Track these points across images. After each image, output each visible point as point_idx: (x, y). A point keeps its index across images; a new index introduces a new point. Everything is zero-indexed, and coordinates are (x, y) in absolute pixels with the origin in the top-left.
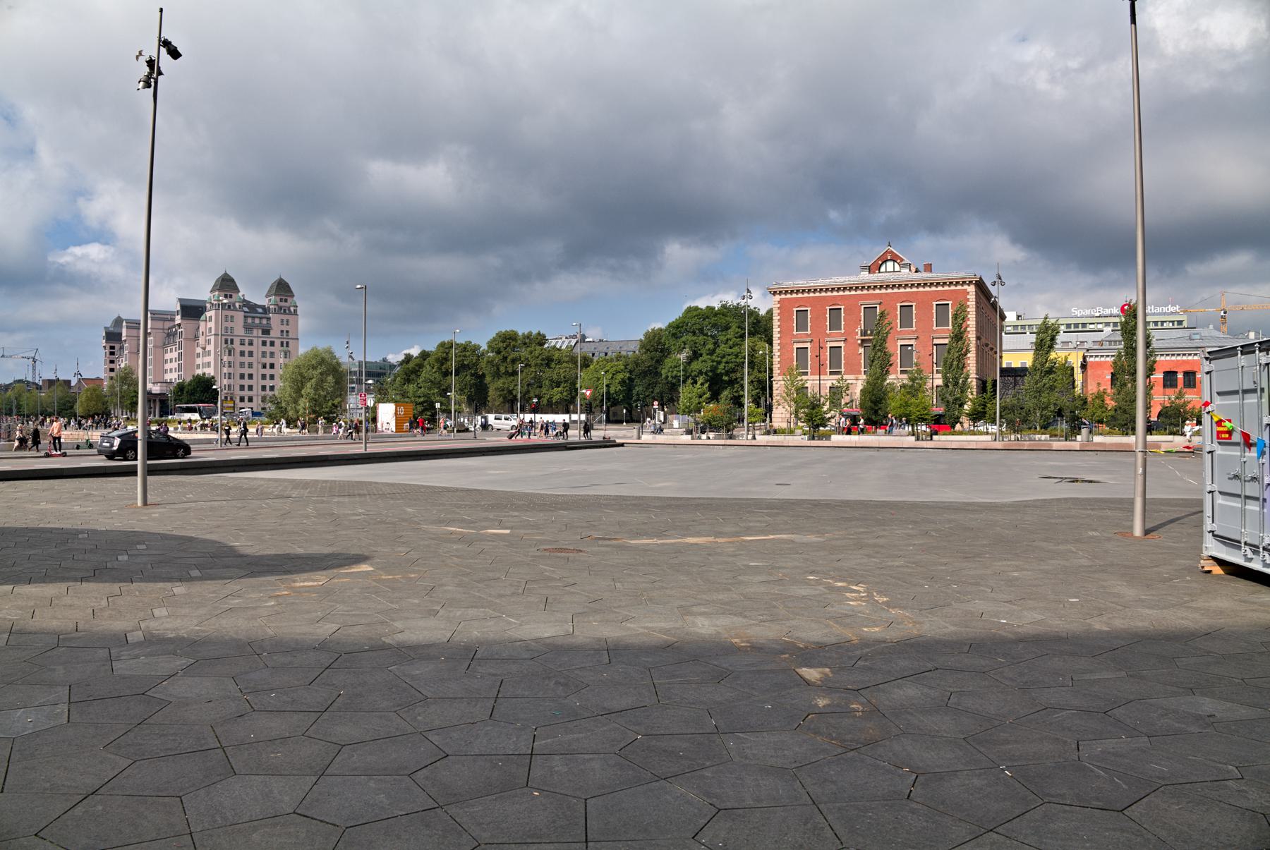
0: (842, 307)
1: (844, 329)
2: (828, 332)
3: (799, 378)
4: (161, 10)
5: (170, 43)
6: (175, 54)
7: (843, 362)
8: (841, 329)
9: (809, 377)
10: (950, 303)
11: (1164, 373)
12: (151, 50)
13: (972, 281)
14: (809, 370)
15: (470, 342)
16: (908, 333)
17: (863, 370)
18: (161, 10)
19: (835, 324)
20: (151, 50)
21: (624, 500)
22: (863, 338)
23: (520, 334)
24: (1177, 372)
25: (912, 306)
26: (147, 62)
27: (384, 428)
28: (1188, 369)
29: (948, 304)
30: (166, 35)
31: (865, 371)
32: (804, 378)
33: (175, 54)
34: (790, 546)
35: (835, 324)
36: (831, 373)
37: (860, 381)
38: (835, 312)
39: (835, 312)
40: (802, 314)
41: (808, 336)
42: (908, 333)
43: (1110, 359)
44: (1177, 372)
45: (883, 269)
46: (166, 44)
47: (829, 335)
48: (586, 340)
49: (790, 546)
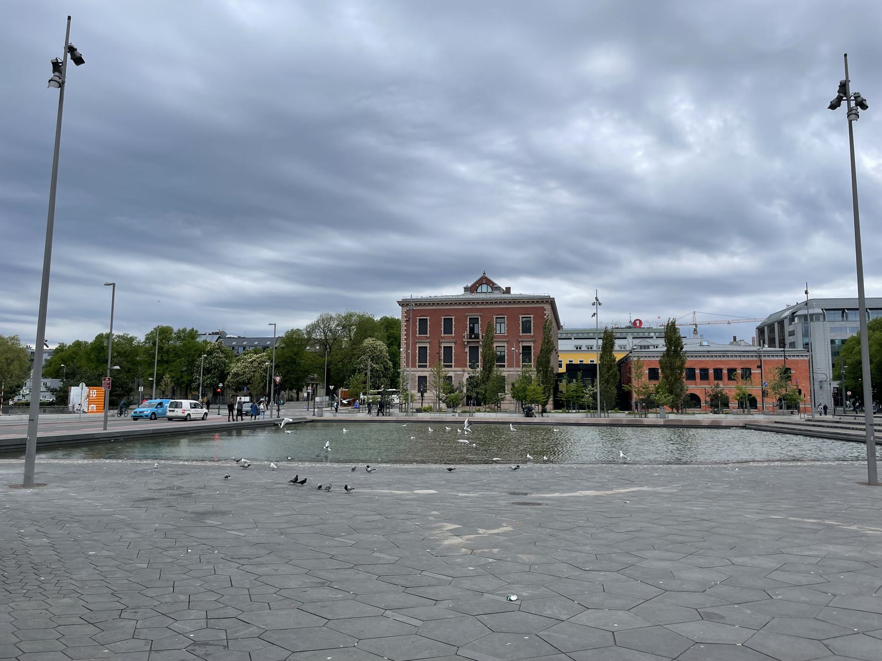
0: (453, 317)
1: (533, 332)
2: (442, 335)
3: (443, 369)
4: (69, 18)
5: (76, 50)
6: (79, 61)
7: (453, 358)
8: (452, 334)
9: (453, 369)
10: (428, 318)
11: (649, 369)
12: (59, 53)
13: (548, 301)
14: (453, 364)
15: (102, 334)
16: (527, 337)
17: (468, 364)
18: (69, 18)
19: (448, 330)
20: (59, 53)
21: (194, 468)
22: (469, 340)
23: (175, 330)
24: (695, 369)
25: (504, 318)
26: (53, 63)
27: (75, 409)
28: (703, 366)
29: (427, 319)
30: (73, 42)
31: (469, 365)
32: (501, 369)
33: (79, 61)
34: (693, 473)
35: (448, 330)
36: (419, 366)
37: (466, 372)
38: (448, 322)
39: (448, 322)
40: (423, 322)
41: (427, 338)
42: (527, 337)
43: (658, 359)
44: (695, 369)
45: (479, 290)
46: (71, 50)
47: (442, 338)
48: (227, 336)
49: (693, 473)
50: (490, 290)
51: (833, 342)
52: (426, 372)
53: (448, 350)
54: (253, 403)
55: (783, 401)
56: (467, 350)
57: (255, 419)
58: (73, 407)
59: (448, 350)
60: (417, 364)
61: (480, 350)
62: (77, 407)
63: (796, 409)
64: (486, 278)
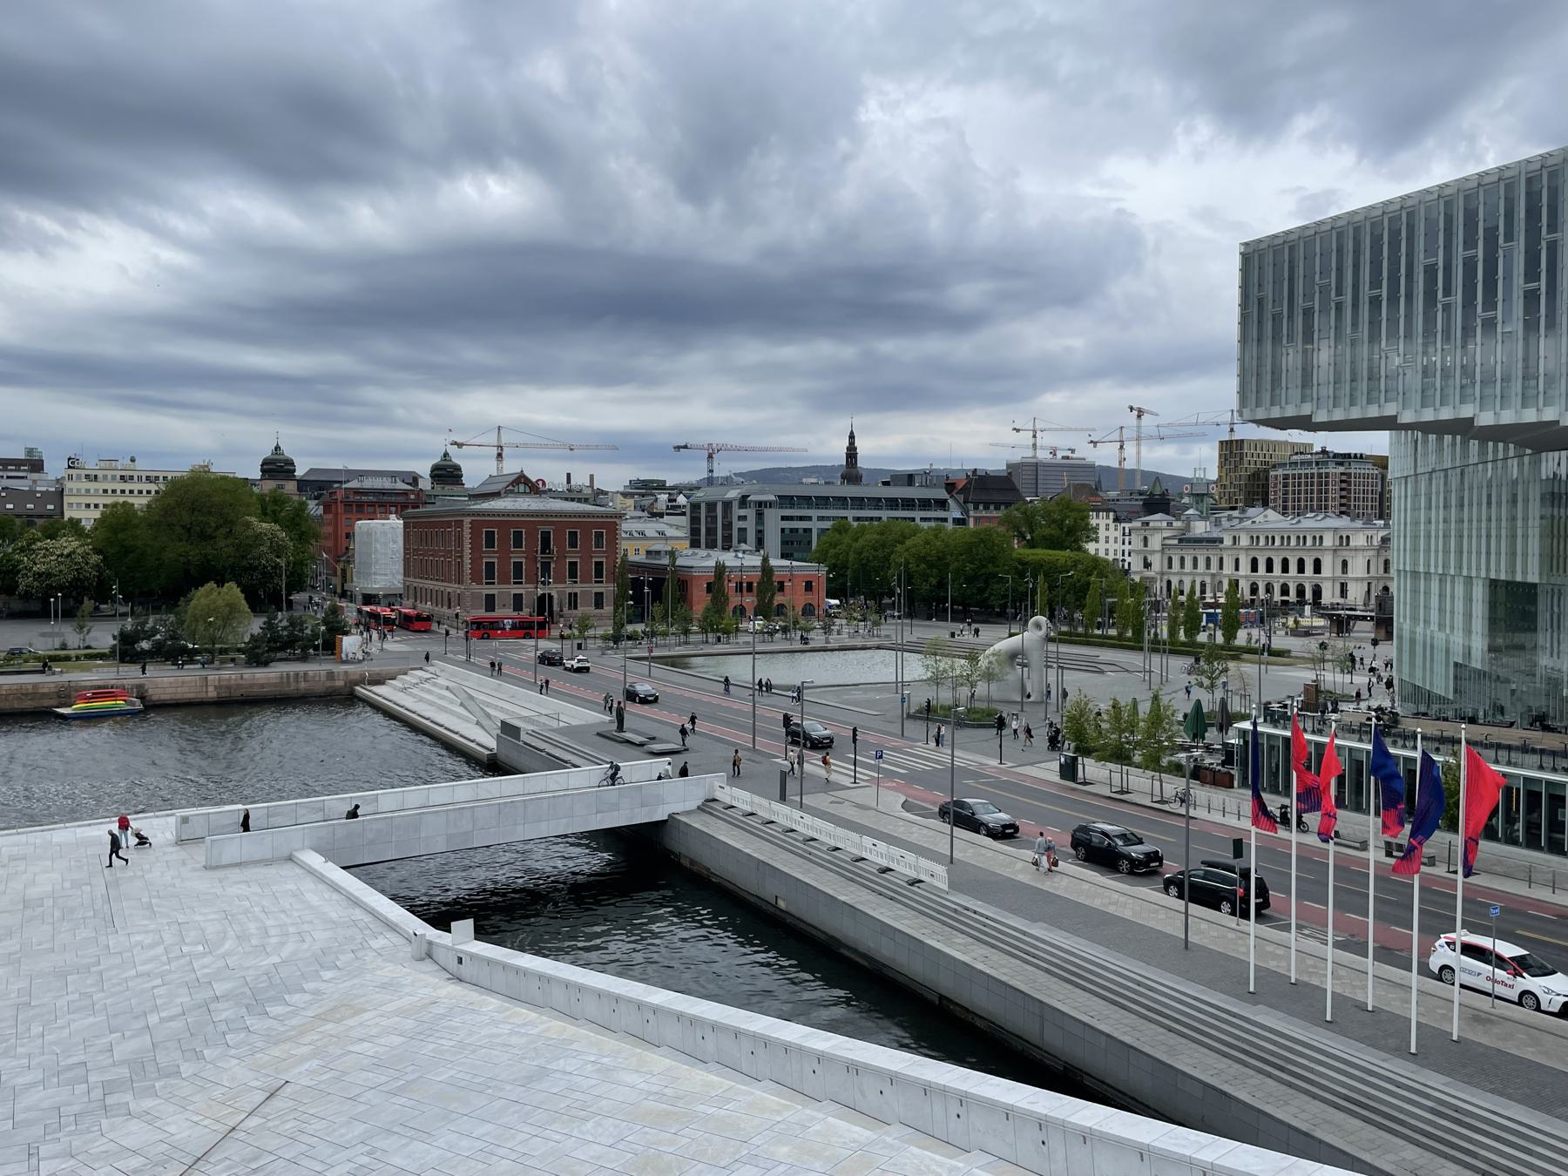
9: (524, 585)
19: (518, 544)
35: (518, 544)
36: (487, 583)
38: (518, 535)
39: (518, 535)
50: (528, 490)
51: (783, 530)
52: (577, 589)
53: (518, 566)
54: (1542, 480)
55: (1421, 570)
56: (539, 565)
57: (1124, 528)
58: (347, 656)
59: (518, 566)
60: (484, 581)
61: (553, 565)
62: (350, 655)
63: (1381, 518)
64: (525, 477)
